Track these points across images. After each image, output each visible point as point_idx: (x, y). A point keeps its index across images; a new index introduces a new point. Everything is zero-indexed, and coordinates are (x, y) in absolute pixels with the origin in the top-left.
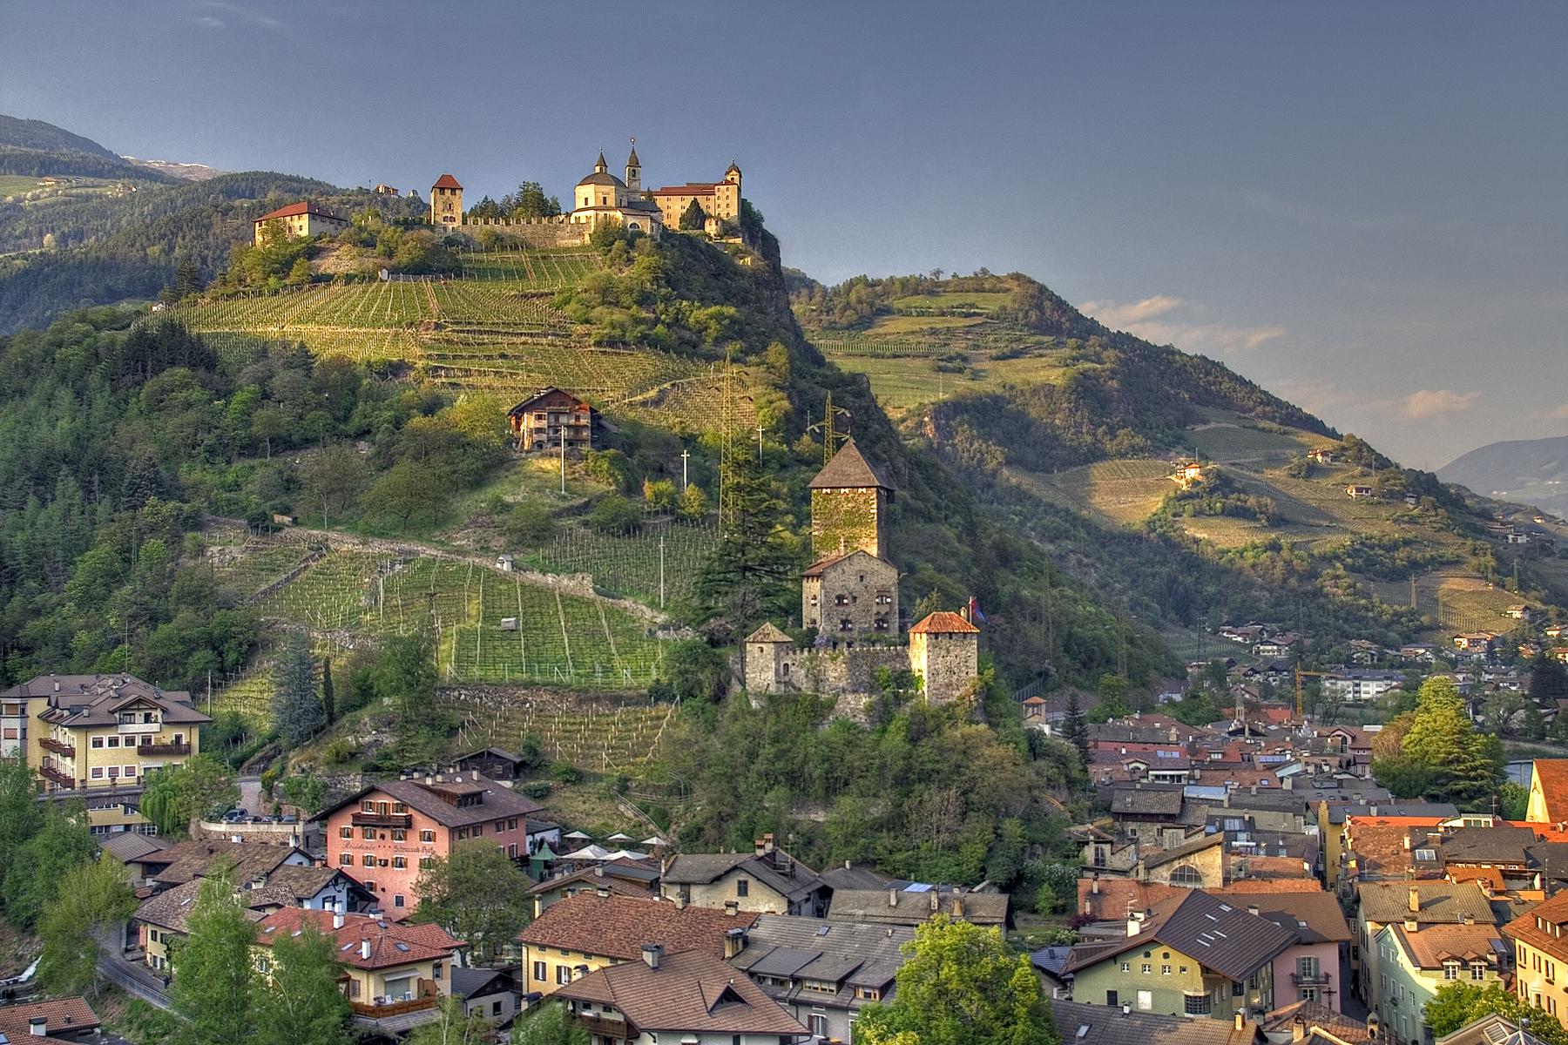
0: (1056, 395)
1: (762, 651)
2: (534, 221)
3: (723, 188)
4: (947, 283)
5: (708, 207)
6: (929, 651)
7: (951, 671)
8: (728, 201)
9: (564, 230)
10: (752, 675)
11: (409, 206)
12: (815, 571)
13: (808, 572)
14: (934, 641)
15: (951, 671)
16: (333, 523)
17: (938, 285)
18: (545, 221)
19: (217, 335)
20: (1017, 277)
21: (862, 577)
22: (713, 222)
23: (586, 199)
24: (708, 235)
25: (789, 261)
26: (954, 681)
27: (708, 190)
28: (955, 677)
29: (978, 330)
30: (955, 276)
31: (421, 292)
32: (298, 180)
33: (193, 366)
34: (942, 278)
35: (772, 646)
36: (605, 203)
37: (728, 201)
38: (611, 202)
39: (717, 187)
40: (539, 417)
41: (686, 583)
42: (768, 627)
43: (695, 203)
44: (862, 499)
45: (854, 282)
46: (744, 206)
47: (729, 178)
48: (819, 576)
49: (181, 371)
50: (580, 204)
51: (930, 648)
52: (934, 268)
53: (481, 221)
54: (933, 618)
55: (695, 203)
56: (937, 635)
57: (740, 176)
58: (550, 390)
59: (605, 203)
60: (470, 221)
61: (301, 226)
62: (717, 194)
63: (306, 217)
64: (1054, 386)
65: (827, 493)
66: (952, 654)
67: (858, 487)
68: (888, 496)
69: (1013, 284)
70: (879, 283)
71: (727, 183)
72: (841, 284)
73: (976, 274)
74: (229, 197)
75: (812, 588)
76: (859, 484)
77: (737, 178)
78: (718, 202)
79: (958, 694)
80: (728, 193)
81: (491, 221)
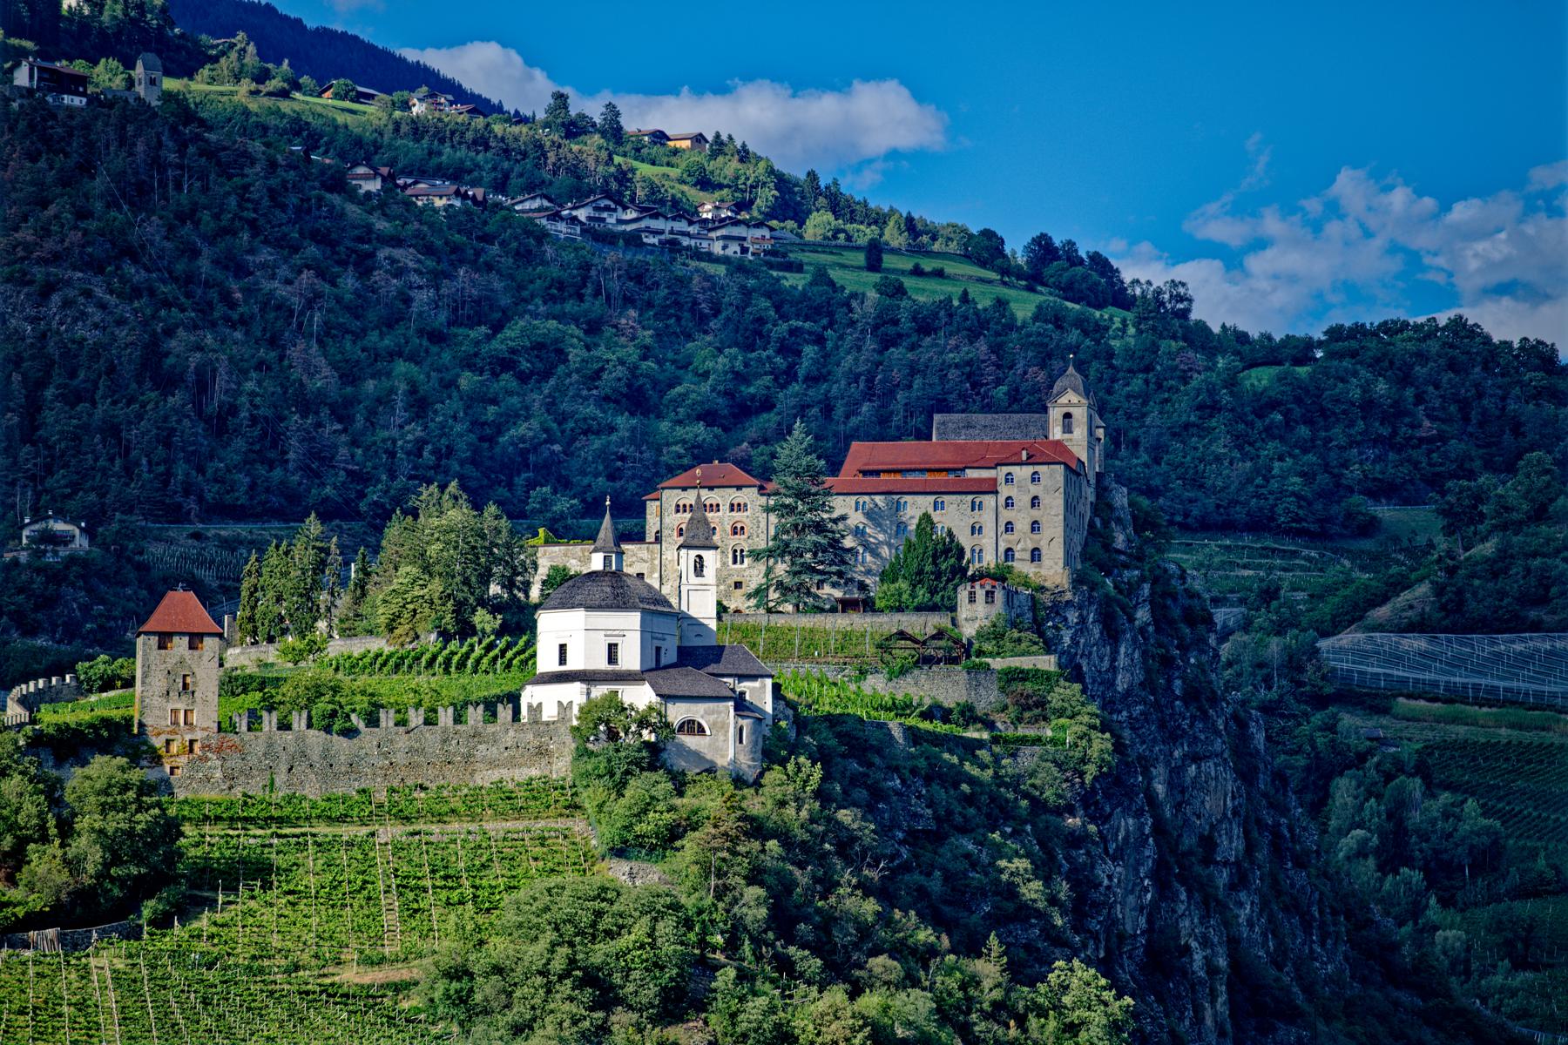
23: (563, 648)
38: (630, 658)
50: (546, 661)
78: (1006, 515)
80: (1034, 490)
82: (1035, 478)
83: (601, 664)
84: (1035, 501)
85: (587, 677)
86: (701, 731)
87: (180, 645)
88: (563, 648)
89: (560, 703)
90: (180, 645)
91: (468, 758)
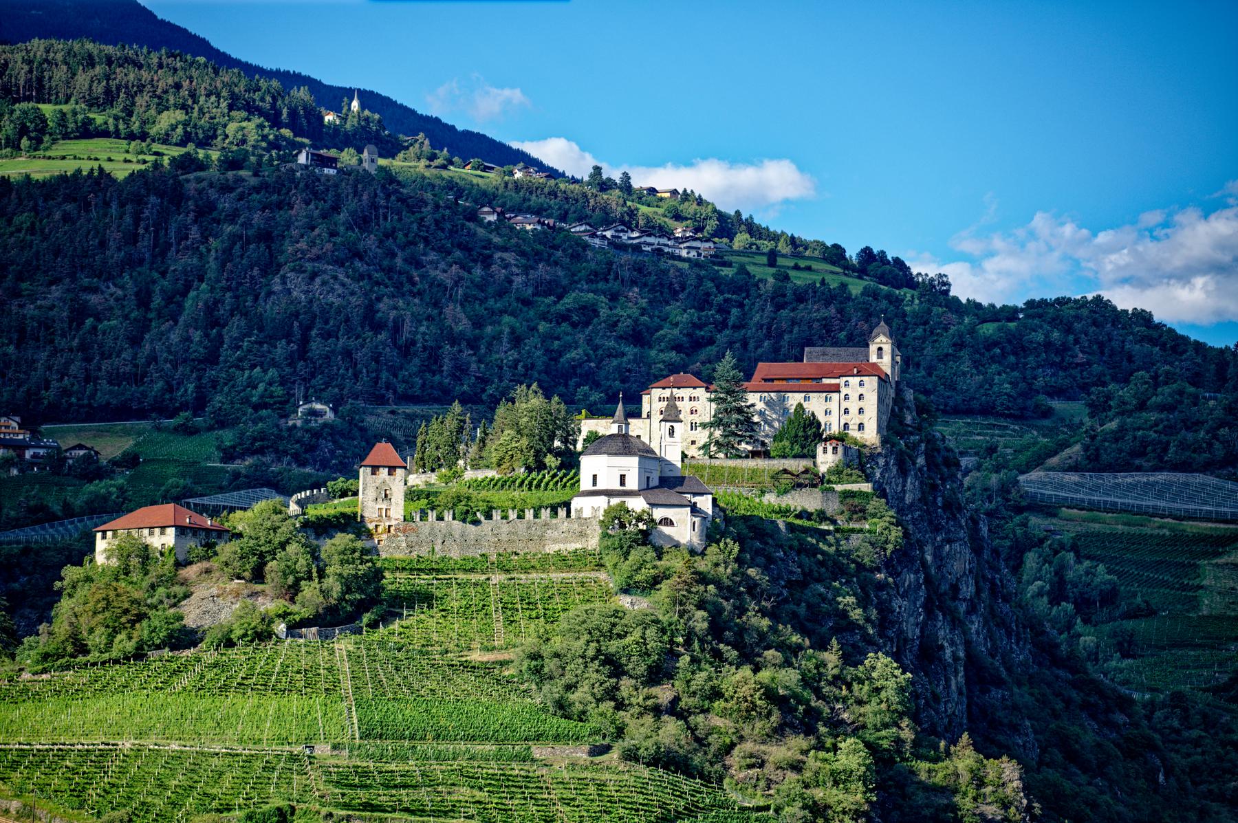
23: (595, 477)
36: (622, 483)
37: (861, 404)
38: (633, 483)
50: (585, 484)
78: (845, 404)
80: (861, 390)
82: (861, 384)
84: (861, 397)
85: (609, 493)
86: (672, 523)
87: (384, 472)
88: (595, 477)
90: (384, 472)
91: (541, 537)
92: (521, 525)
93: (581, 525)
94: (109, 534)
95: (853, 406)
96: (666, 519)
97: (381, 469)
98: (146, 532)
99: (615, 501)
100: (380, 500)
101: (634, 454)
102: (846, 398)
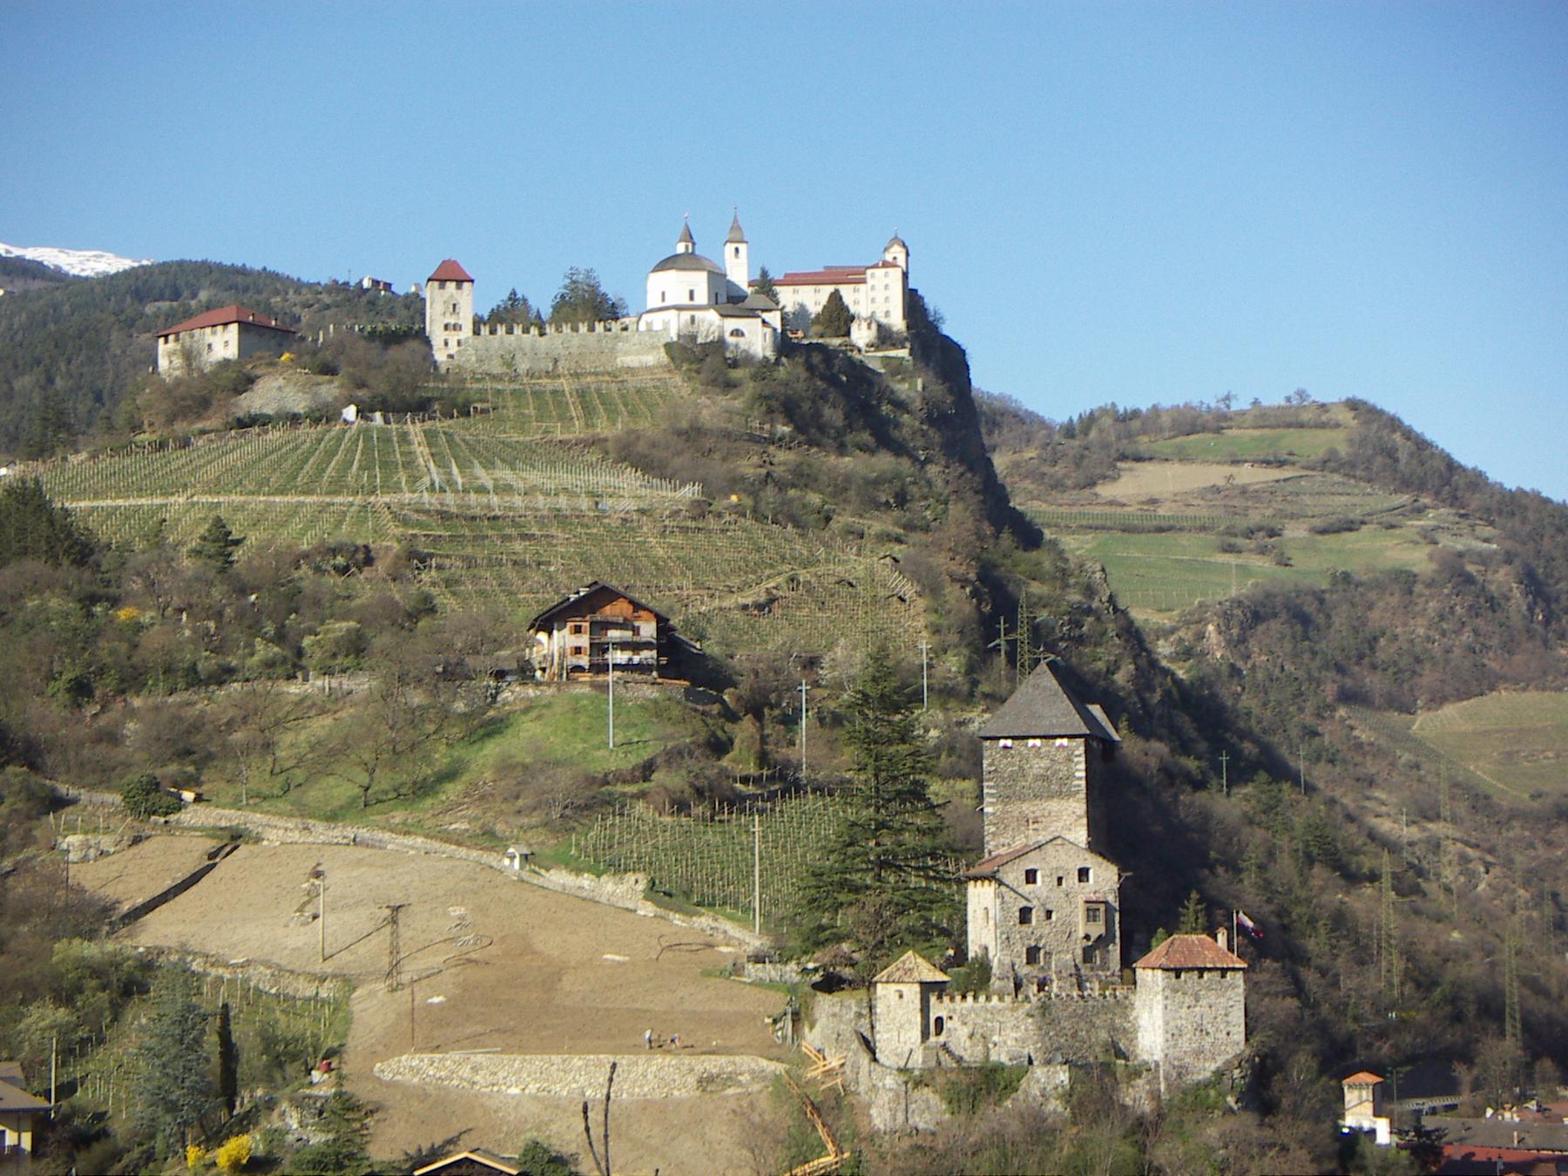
0: (1418, 588)
1: (901, 996)
2: (583, 328)
3: (880, 272)
4: (1242, 413)
5: (856, 302)
6: (1167, 998)
7: (1201, 1030)
8: (888, 293)
9: (627, 341)
10: (886, 1036)
11: (407, 307)
12: (986, 869)
13: (972, 872)
14: (1174, 980)
15: (1201, 1030)
16: (260, 798)
17: (1225, 417)
18: (599, 327)
19: (111, 513)
20: (1354, 405)
21: (1060, 880)
22: (864, 325)
23: (663, 294)
24: (853, 347)
25: (986, 379)
26: (1207, 1046)
27: (856, 276)
28: (1209, 1039)
29: (1289, 487)
30: (1256, 402)
31: (404, 438)
32: (242, 271)
33: (53, 557)
34: (1235, 406)
35: (1159, 973)
36: (692, 298)
37: (888, 293)
38: (702, 297)
39: (869, 272)
40: (578, 630)
41: (788, 889)
42: (910, 958)
43: (836, 298)
44: (1061, 756)
45: (1096, 414)
46: (913, 303)
47: (889, 257)
48: (992, 877)
49: (35, 567)
50: (653, 301)
51: (1168, 992)
52: (1222, 394)
53: (501, 330)
54: (1172, 943)
55: (836, 298)
56: (1178, 972)
57: (907, 254)
58: (594, 588)
59: (692, 298)
60: (485, 330)
61: (223, 344)
62: (870, 282)
63: (234, 328)
64: (1415, 576)
65: (1005, 747)
66: (1203, 1002)
67: (1055, 737)
68: (1104, 750)
69: (1346, 417)
70: (1136, 414)
71: (886, 265)
72: (1075, 419)
73: (1288, 399)
74: (141, 301)
75: (980, 897)
76: (1056, 732)
77: (901, 261)
78: (873, 294)
79: (1213, 1067)
80: (887, 281)
81: (518, 330)
82: (886, 275)
83: (686, 301)
84: (886, 287)
85: (679, 308)
86: (743, 335)
87: (451, 286)
88: (663, 294)
89: (514, 293)
90: (451, 286)
91: (613, 350)
92: (592, 337)
93: (651, 337)
94: (171, 338)
95: (880, 298)
96: (737, 330)
97: (448, 284)
98: (208, 330)
99: (686, 315)
100: (448, 315)
101: (703, 270)
102: (873, 288)
